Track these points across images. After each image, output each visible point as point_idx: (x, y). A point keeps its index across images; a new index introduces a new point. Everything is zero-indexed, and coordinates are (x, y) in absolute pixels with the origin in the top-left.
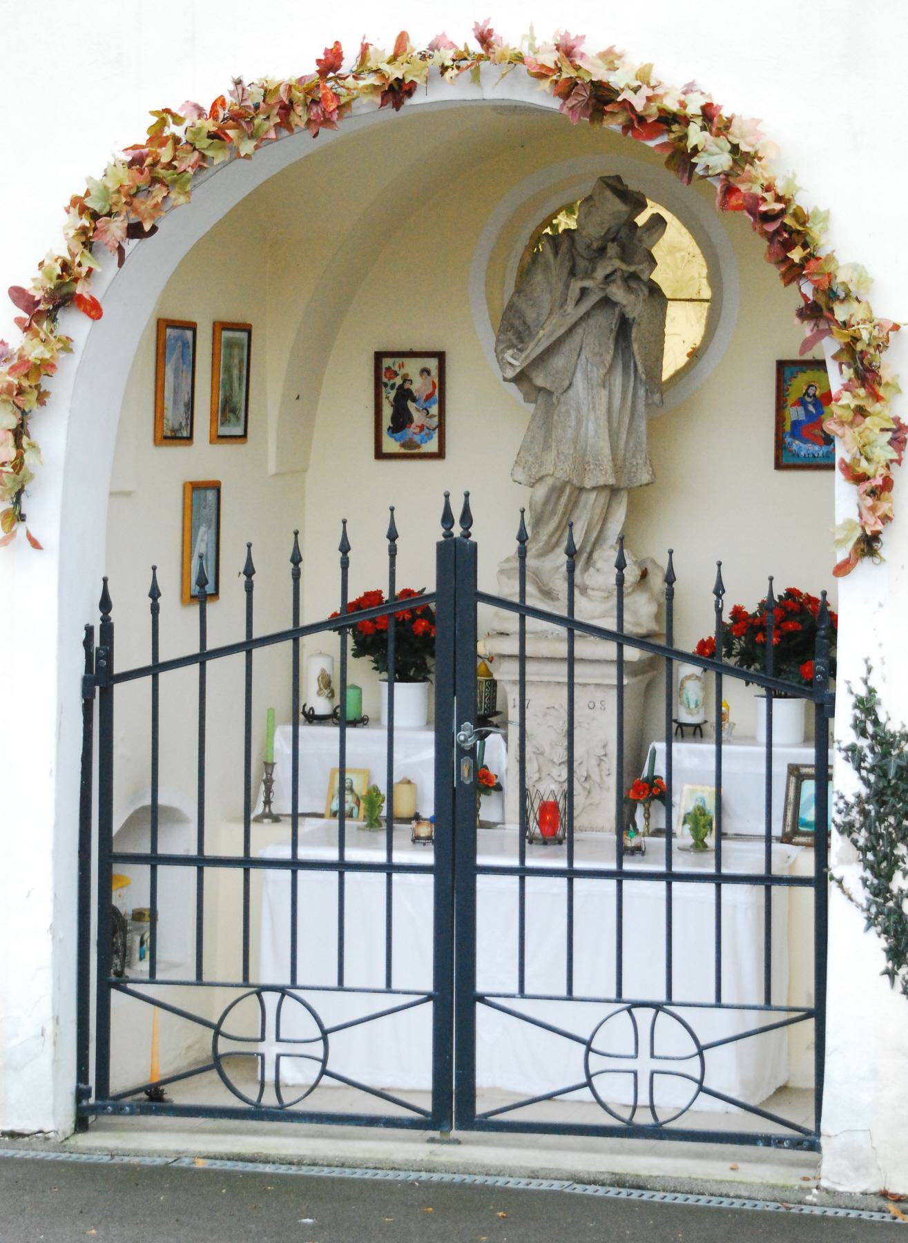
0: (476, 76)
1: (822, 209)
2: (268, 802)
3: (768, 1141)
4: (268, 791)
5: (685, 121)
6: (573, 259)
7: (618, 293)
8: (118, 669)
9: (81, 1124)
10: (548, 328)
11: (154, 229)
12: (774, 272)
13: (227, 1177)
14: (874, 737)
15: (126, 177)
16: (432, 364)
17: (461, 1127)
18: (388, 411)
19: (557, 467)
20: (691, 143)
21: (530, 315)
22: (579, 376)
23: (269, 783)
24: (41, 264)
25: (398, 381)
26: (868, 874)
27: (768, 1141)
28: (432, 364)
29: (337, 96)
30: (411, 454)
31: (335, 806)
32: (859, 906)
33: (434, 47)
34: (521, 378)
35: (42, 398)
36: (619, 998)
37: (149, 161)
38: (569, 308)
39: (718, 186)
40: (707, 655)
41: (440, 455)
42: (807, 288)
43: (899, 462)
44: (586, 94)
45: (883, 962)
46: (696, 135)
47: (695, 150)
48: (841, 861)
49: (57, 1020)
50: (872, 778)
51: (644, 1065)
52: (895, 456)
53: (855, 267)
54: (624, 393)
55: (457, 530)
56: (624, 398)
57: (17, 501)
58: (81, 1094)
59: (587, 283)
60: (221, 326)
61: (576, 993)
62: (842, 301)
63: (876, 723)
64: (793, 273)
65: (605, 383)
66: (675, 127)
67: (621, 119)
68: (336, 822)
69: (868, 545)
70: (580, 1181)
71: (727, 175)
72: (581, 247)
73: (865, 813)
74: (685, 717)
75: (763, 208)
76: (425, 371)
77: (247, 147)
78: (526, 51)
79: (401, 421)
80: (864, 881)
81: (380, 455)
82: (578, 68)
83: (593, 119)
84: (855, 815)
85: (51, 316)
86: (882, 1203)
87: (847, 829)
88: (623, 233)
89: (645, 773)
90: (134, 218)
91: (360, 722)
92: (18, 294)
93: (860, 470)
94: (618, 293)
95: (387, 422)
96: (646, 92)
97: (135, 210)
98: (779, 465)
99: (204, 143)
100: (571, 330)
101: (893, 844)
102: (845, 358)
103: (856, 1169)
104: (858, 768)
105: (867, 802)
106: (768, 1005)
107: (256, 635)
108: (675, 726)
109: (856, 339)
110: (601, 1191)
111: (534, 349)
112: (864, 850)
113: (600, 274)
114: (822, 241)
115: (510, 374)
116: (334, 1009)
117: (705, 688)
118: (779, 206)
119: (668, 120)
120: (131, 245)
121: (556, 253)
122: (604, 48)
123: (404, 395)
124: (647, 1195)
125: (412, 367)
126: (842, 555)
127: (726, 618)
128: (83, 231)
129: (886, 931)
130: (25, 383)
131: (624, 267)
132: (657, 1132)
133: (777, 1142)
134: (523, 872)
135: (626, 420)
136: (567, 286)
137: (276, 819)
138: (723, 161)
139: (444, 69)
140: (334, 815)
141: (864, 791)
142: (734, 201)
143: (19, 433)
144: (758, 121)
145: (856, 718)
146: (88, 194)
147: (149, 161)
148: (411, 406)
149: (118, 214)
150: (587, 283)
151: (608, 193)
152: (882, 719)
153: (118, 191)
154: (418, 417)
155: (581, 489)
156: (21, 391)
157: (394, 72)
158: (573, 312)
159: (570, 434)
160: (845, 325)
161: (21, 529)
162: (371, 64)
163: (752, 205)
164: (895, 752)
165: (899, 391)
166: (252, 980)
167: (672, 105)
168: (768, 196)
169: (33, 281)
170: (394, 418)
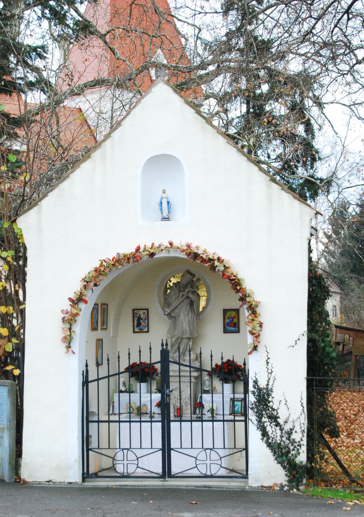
0: (169, 252)
1: (243, 278)
2: (113, 411)
3: (236, 477)
4: (113, 408)
5: (214, 260)
6: (179, 288)
7: (190, 295)
8: (89, 380)
9: (83, 481)
10: (175, 303)
11: (99, 284)
12: (234, 292)
13: (119, 489)
14: (257, 389)
15: (94, 274)
16: (146, 311)
17: (168, 478)
18: (136, 322)
19: (178, 333)
20: (215, 265)
21: (170, 301)
22: (182, 313)
23: (113, 406)
24: (75, 293)
25: (138, 315)
26: (257, 418)
27: (236, 477)
28: (146, 311)
29: (140, 256)
30: (141, 331)
31: (128, 411)
32: (255, 425)
33: (160, 246)
34: (169, 315)
35: (75, 321)
36: (203, 448)
37: (98, 270)
38: (180, 298)
39: (221, 274)
40: (210, 374)
41: (148, 332)
42: (241, 295)
43: (261, 330)
44: (193, 255)
45: (261, 437)
46: (216, 263)
47: (216, 266)
48: (251, 415)
49: (79, 457)
50: (257, 397)
51: (208, 462)
52: (260, 329)
53: (250, 290)
54: (192, 316)
55: (165, 347)
56: (191, 318)
57: (69, 343)
58: (83, 474)
59: (184, 293)
60: (103, 304)
61: (193, 447)
62: (248, 297)
63: (258, 386)
64: (238, 291)
65: (188, 315)
66: (212, 262)
67: (200, 260)
68: (129, 414)
69: (255, 348)
70: (197, 487)
71: (223, 271)
72: (181, 285)
73: (256, 405)
74: (206, 389)
75: (231, 278)
76: (144, 313)
77: (120, 267)
78: (180, 247)
79: (139, 324)
80: (256, 419)
81: (134, 332)
82: (191, 250)
83: (194, 260)
84: (254, 405)
85: (77, 303)
86: (262, 488)
87: (252, 409)
88: (191, 282)
89: (198, 401)
90: (95, 282)
91: (133, 392)
92: (70, 299)
93: (253, 332)
94: (190, 295)
95: (136, 324)
96: (205, 254)
97: (96, 281)
98: (224, 332)
99: (111, 266)
100: (180, 304)
101: (262, 411)
102: (249, 309)
103: (256, 481)
104: (254, 396)
105: (257, 402)
106: (235, 448)
107: (110, 374)
108: (203, 391)
109: (251, 305)
110: (202, 488)
111: (172, 308)
112: (256, 413)
113: (186, 291)
114: (243, 285)
115: (167, 313)
116: (139, 453)
117: (210, 382)
118: (234, 278)
119: (210, 260)
120: (94, 288)
121: (176, 287)
122: (196, 246)
123: (139, 319)
124: (212, 489)
125: (141, 312)
126: (249, 350)
127: (214, 366)
128: (85, 285)
129: (261, 430)
130: (72, 318)
131: (192, 290)
132: (212, 476)
133: (238, 477)
134: (234, 421)
135: (192, 323)
136: (179, 294)
137: (115, 414)
138: (222, 268)
139: (162, 250)
140: (128, 413)
141: (256, 400)
142: (225, 276)
143: (70, 329)
144: (229, 260)
145: (254, 385)
146: (85, 277)
147: (98, 270)
148: (141, 321)
149: (92, 282)
150: (184, 293)
151: (188, 274)
152: (259, 385)
153: (92, 277)
154: (143, 323)
155: (182, 338)
156: (71, 320)
157: (152, 251)
158: (180, 299)
159: (180, 326)
160: (249, 302)
161: (70, 350)
162: (147, 249)
163: (229, 278)
164: (262, 392)
165: (260, 315)
166: (121, 447)
167: (211, 257)
168: (232, 275)
169: (73, 296)
170: (137, 324)
